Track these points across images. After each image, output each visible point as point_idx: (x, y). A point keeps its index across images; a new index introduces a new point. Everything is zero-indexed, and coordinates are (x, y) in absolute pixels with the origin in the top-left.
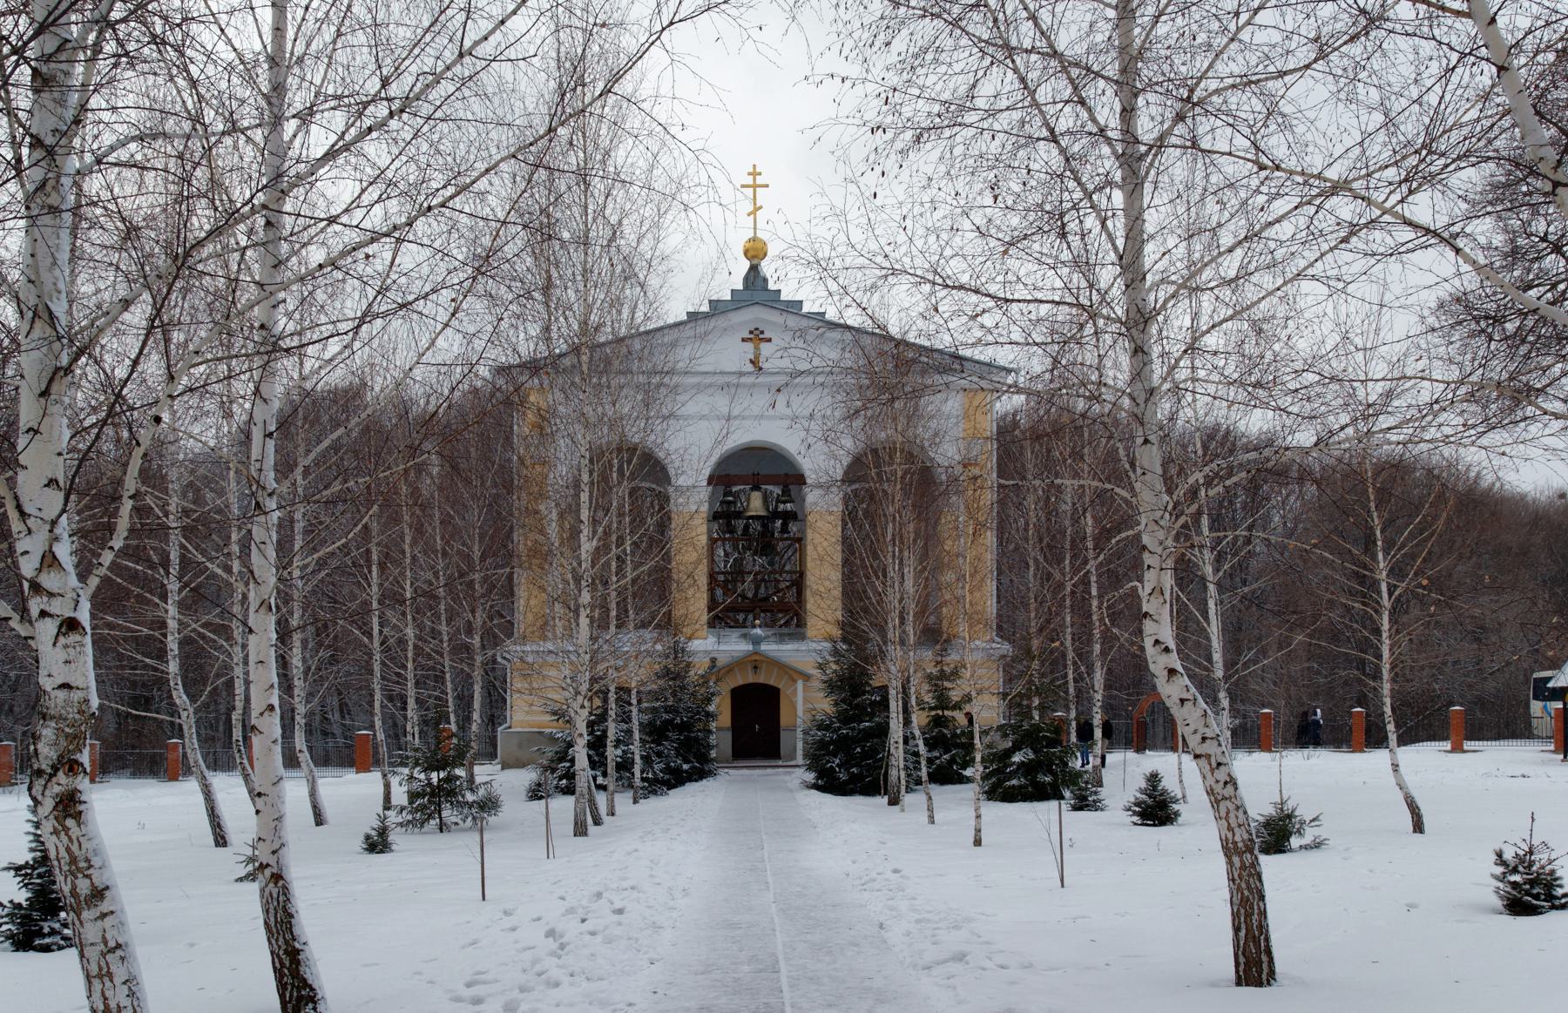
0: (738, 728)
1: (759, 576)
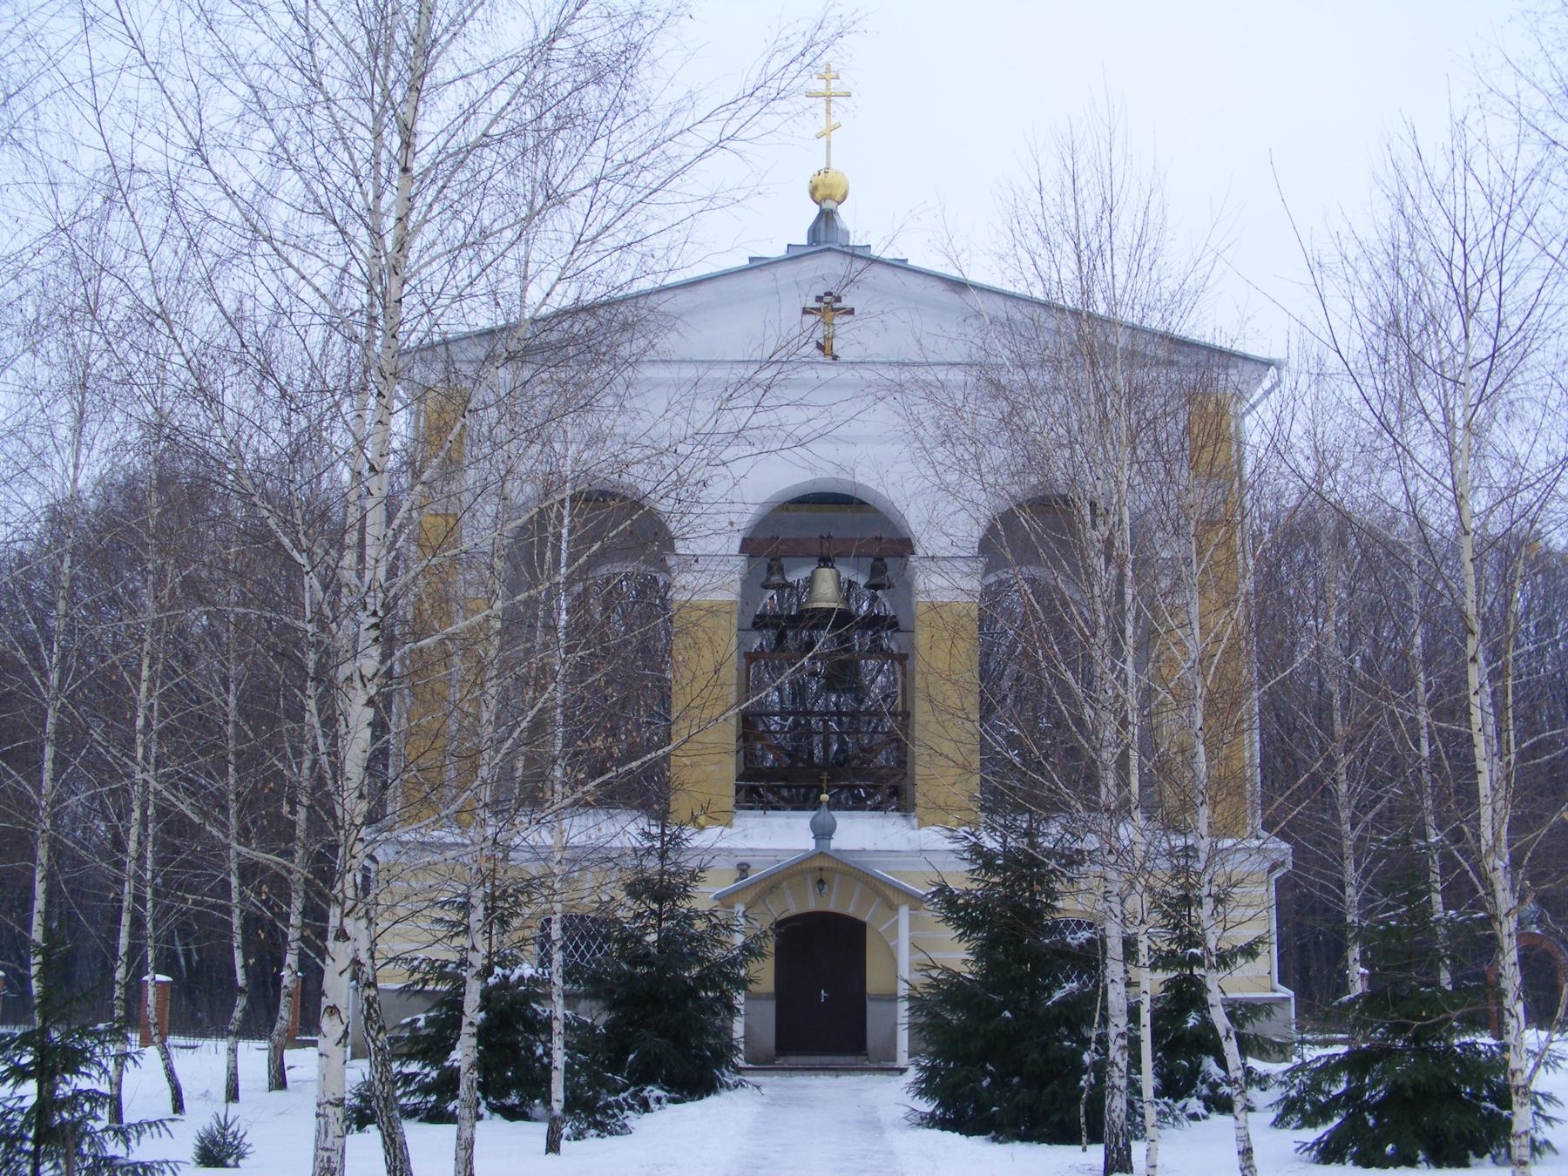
0: (788, 996)
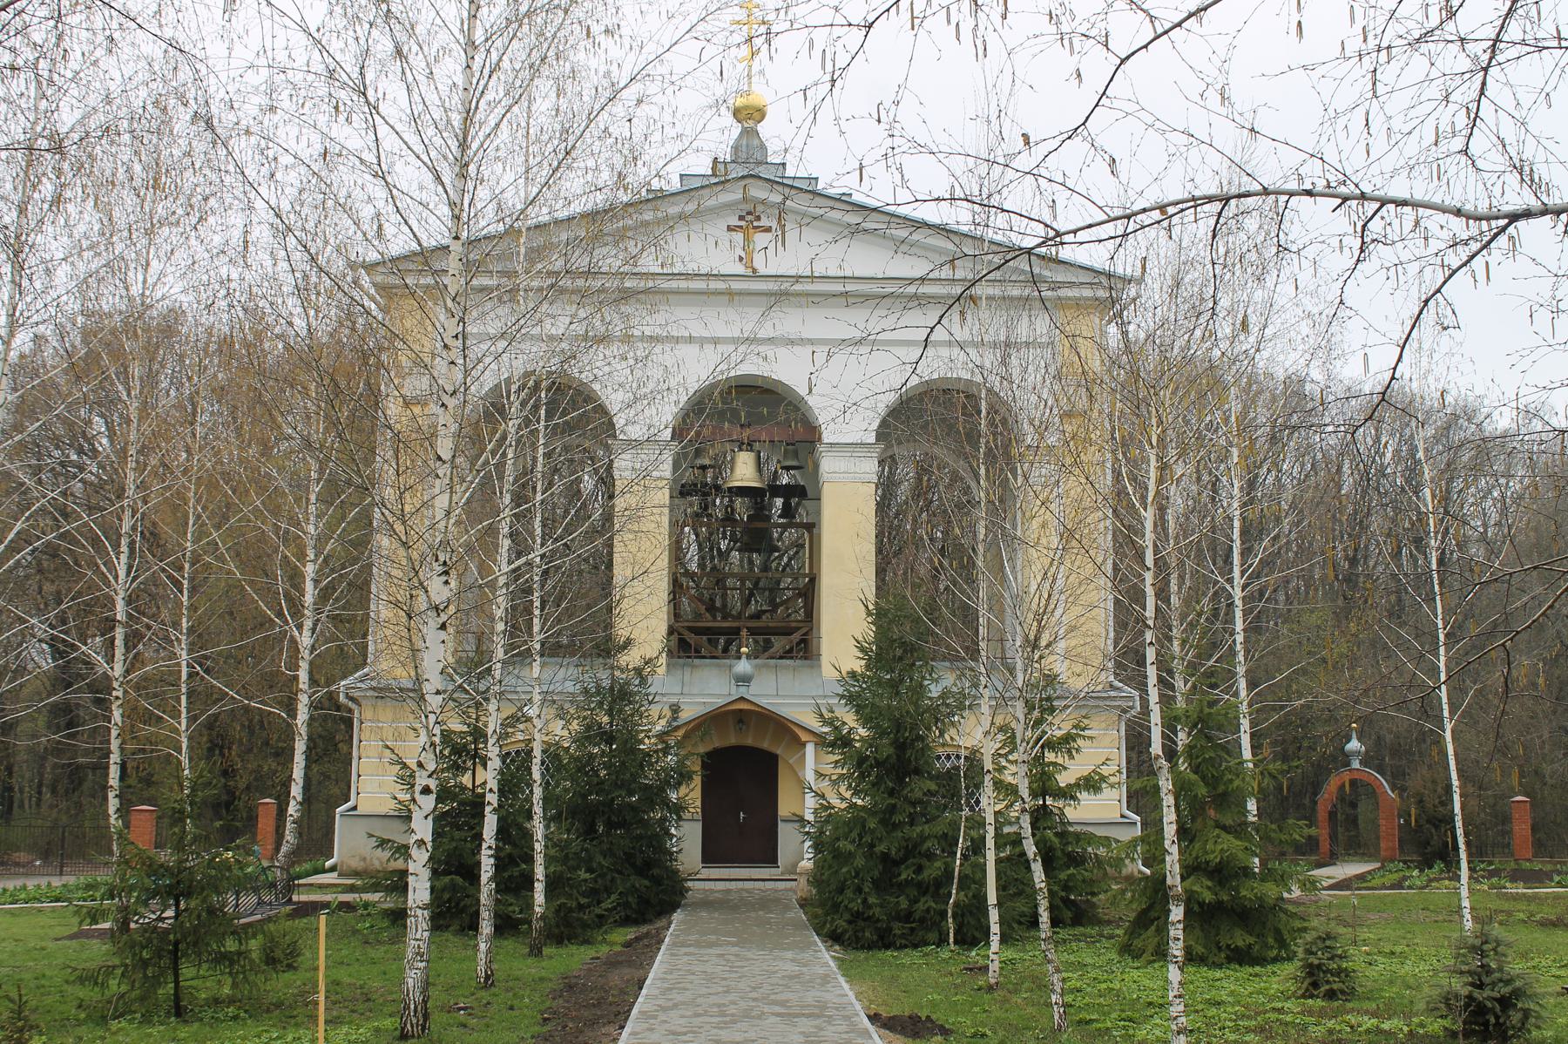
1: (746, 584)
